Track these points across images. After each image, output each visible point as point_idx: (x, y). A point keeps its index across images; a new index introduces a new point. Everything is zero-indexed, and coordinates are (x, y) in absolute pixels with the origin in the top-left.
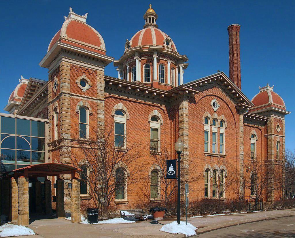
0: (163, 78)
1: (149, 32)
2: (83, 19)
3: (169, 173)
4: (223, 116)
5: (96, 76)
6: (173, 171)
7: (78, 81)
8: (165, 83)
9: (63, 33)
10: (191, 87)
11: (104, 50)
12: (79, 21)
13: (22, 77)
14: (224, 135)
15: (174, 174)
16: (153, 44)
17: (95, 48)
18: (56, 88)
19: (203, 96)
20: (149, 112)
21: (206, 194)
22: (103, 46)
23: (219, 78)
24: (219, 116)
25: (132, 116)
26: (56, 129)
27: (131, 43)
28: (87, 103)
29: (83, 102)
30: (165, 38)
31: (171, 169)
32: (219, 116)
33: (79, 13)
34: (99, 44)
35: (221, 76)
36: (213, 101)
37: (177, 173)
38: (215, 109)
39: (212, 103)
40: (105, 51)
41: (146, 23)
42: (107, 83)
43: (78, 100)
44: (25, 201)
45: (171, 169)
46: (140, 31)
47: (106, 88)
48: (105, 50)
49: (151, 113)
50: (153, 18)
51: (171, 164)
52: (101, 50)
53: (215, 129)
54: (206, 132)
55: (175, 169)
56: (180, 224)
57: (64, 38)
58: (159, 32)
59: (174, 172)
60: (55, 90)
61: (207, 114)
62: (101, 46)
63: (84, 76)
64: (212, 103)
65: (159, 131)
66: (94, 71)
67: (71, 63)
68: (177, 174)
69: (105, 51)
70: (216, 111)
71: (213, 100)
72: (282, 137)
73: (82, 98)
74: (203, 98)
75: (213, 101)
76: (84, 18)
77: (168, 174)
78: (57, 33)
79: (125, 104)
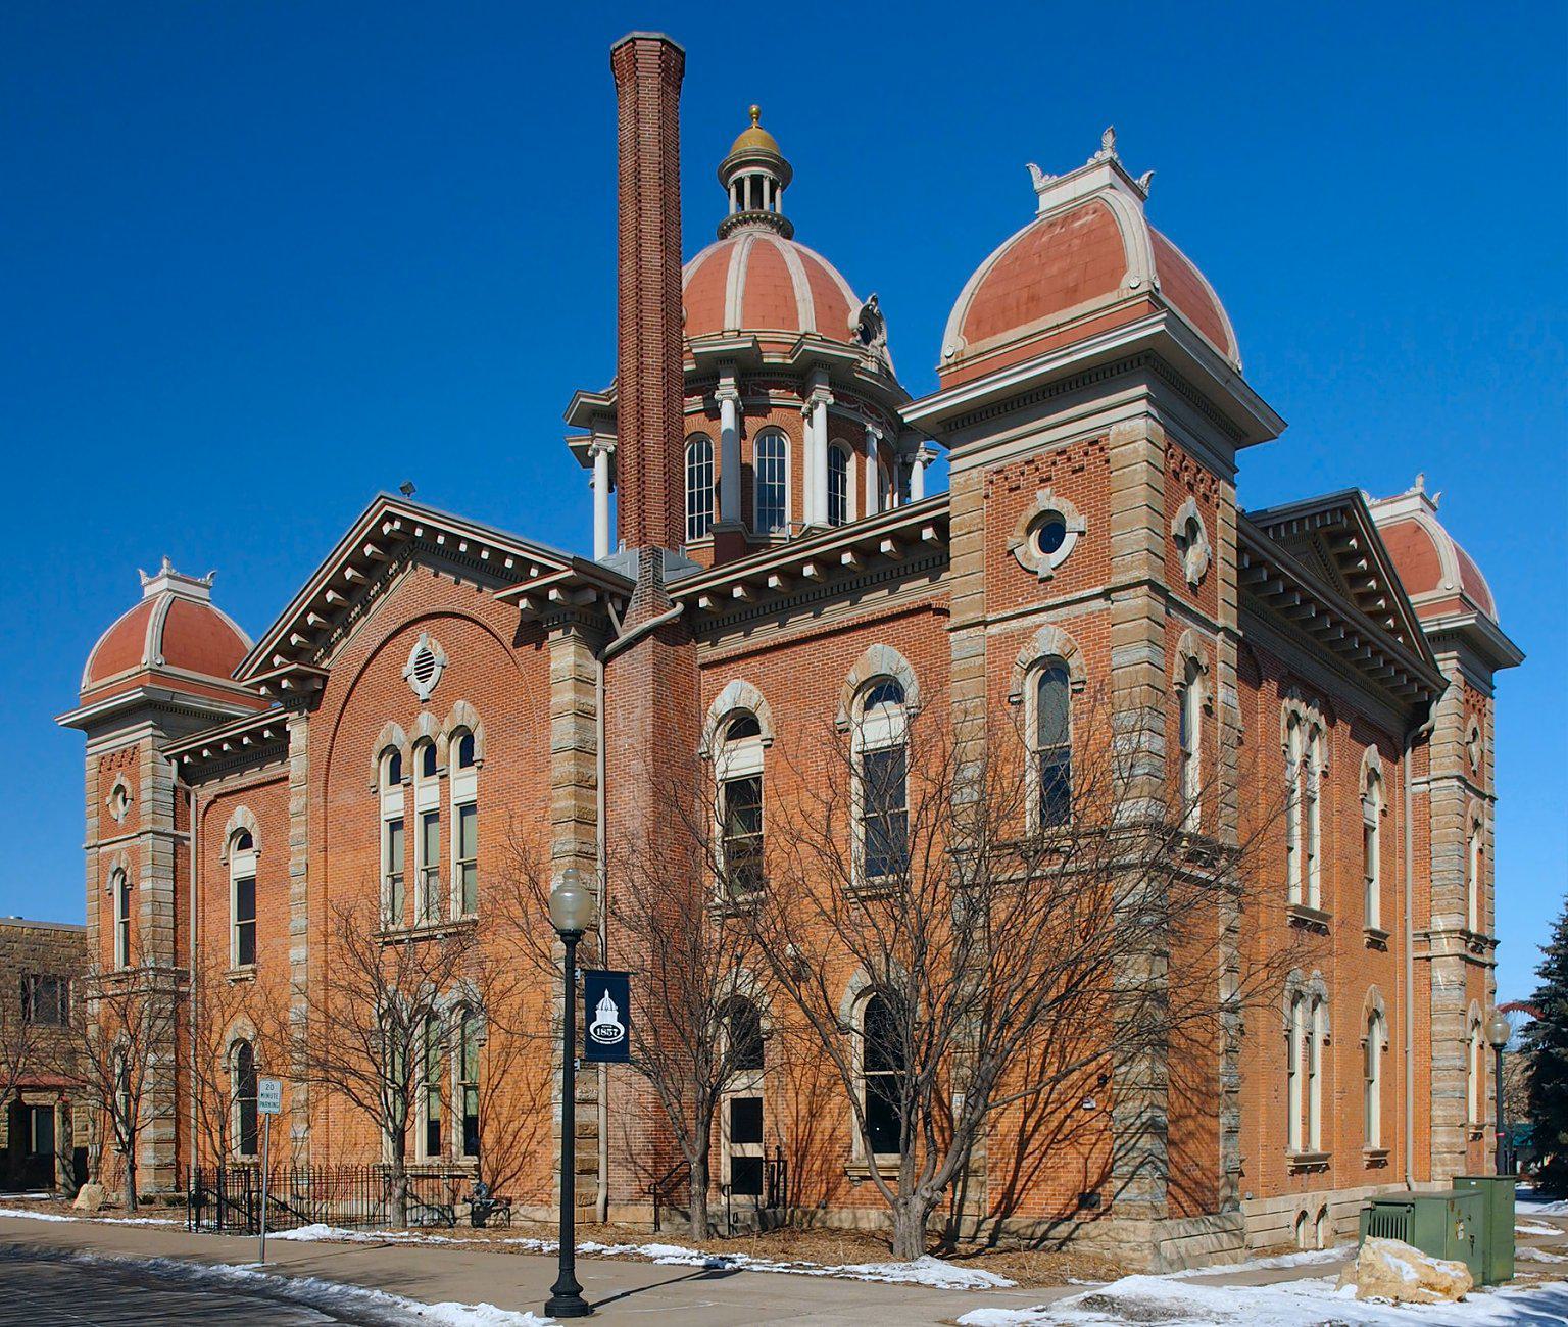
3: (596, 1032)
6: (614, 1027)
10: (277, 660)
16: (726, 327)
35: (390, 518)
41: (733, 210)
45: (607, 1013)
51: (607, 992)
53: (427, 794)
55: (624, 1017)
57: (1135, 292)
59: (622, 1032)
63: (1075, 522)
67: (97, 753)
70: (429, 697)
72: (1106, 595)
78: (868, 379)
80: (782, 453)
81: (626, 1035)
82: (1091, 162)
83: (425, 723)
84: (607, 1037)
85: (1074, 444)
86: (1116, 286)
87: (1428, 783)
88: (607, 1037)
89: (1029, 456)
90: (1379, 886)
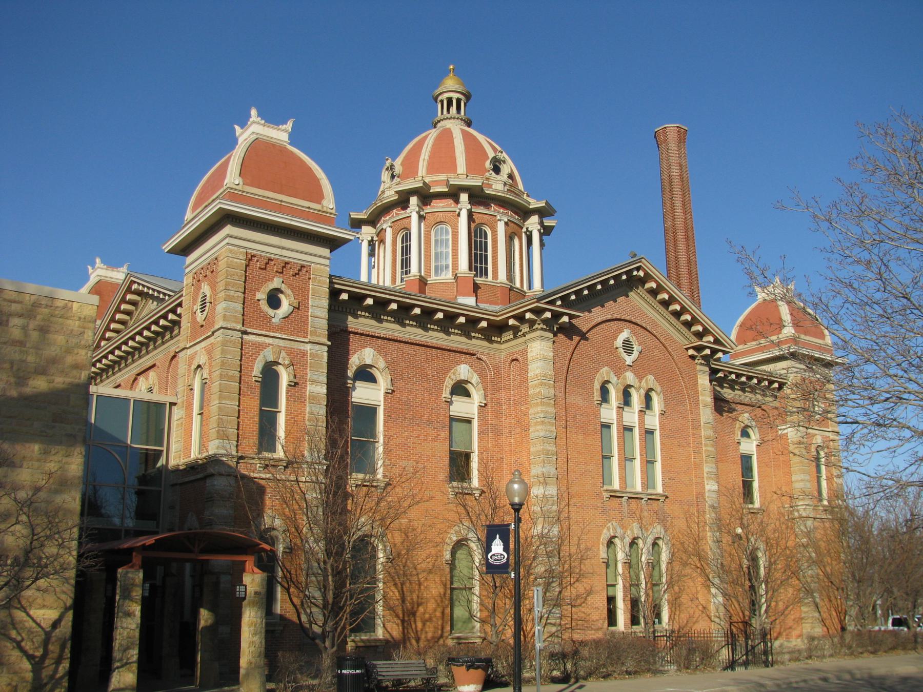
0: (486, 263)
1: (447, 135)
2: (280, 135)
3: (491, 557)
4: (651, 378)
5: (309, 279)
6: (501, 555)
7: (262, 295)
8: (493, 279)
9: (233, 178)
10: (559, 303)
11: (331, 211)
12: (272, 138)
13: (98, 260)
14: (657, 434)
15: (505, 560)
17: (309, 208)
18: (205, 313)
19: (594, 323)
20: (444, 372)
21: (612, 619)
22: (329, 203)
23: (635, 273)
24: (640, 381)
25: (400, 384)
26: (196, 419)
27: (398, 169)
28: (283, 354)
29: (274, 353)
30: (491, 154)
31: (497, 547)
32: (640, 381)
33: (272, 118)
34: (318, 196)
36: (625, 335)
37: (512, 557)
38: (629, 360)
39: (619, 342)
40: (335, 215)
42: (334, 294)
43: (261, 347)
44: (250, 625)
45: (497, 547)
46: (424, 134)
47: (333, 308)
48: (333, 211)
49: (451, 374)
50: (459, 101)
51: (498, 536)
52: (324, 212)
54: (607, 426)
55: (506, 549)
56: (468, 670)
58: (472, 135)
60: (200, 317)
61: (605, 373)
62: (325, 203)
64: (619, 342)
65: (475, 423)
66: (303, 266)
68: (512, 562)
69: (335, 215)
71: (621, 335)
73: (270, 341)
74: (594, 330)
75: (625, 335)
76: (285, 130)
77: (491, 561)
79: (380, 351)
80: (486, 237)
81: (508, 559)
82: (249, 123)
83: (630, 377)
84: (498, 560)
85: (294, 263)
86: (223, 186)
87: (807, 428)
88: (498, 560)
89: (207, 261)
90: (660, 464)
